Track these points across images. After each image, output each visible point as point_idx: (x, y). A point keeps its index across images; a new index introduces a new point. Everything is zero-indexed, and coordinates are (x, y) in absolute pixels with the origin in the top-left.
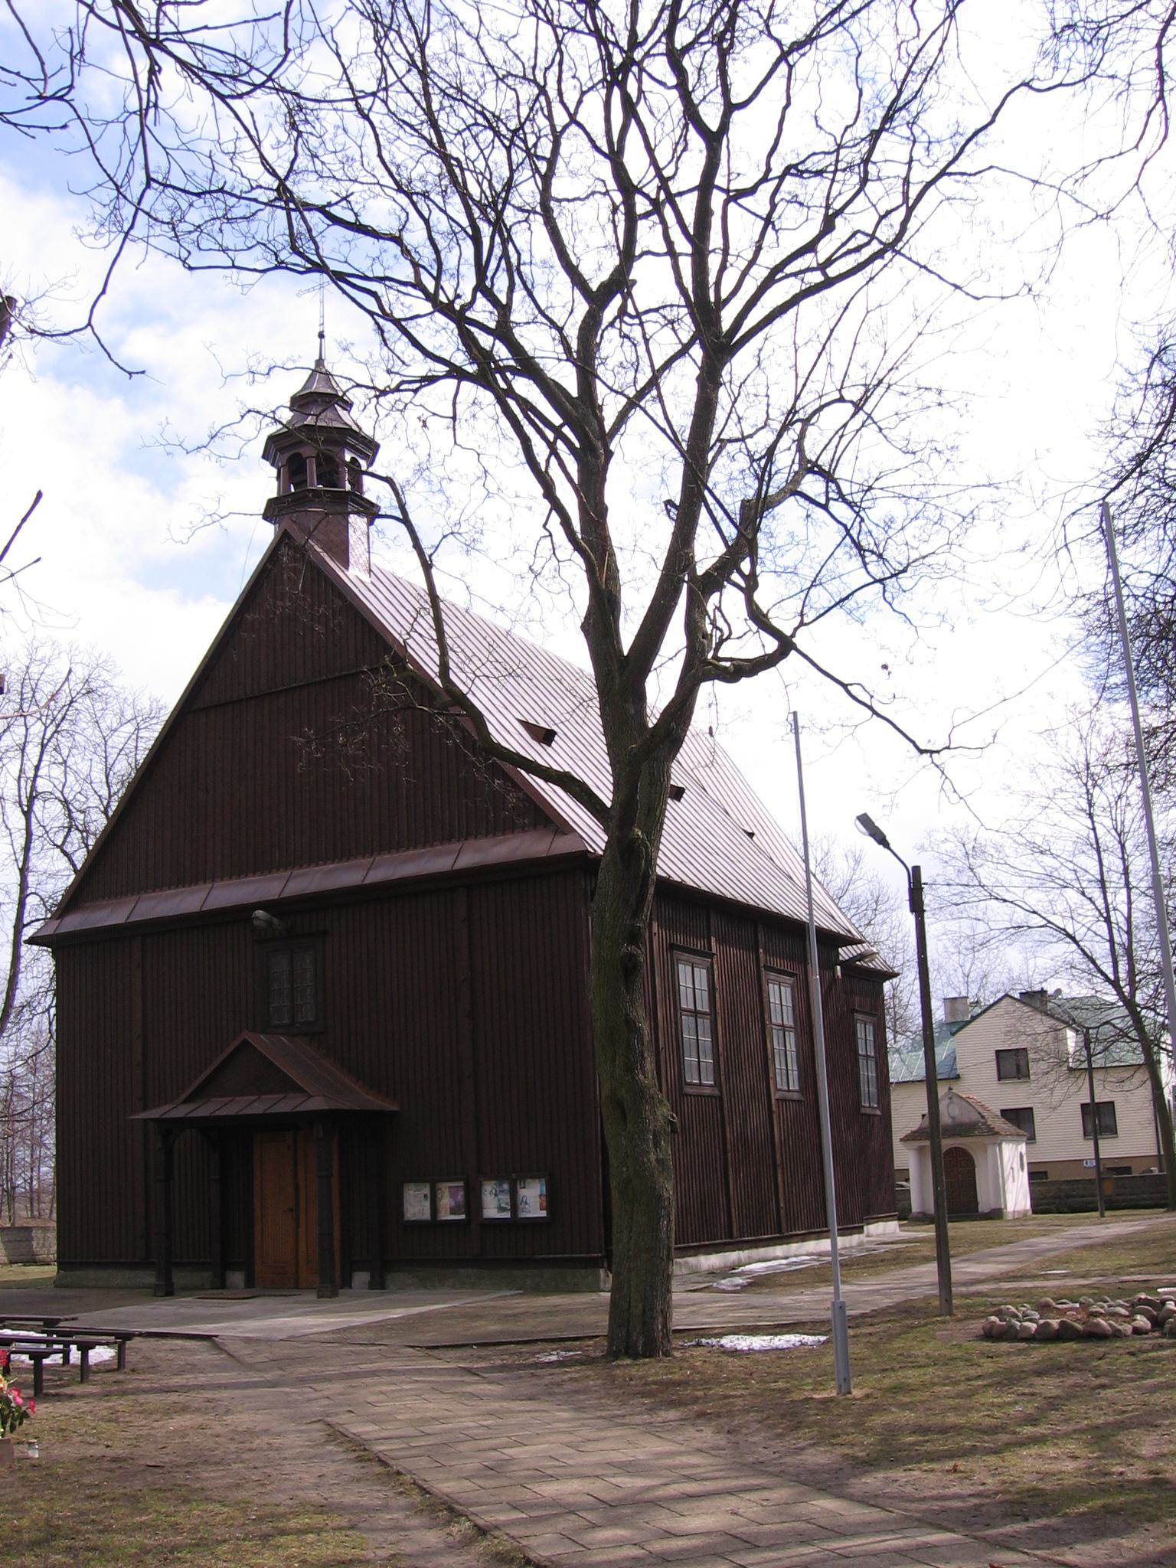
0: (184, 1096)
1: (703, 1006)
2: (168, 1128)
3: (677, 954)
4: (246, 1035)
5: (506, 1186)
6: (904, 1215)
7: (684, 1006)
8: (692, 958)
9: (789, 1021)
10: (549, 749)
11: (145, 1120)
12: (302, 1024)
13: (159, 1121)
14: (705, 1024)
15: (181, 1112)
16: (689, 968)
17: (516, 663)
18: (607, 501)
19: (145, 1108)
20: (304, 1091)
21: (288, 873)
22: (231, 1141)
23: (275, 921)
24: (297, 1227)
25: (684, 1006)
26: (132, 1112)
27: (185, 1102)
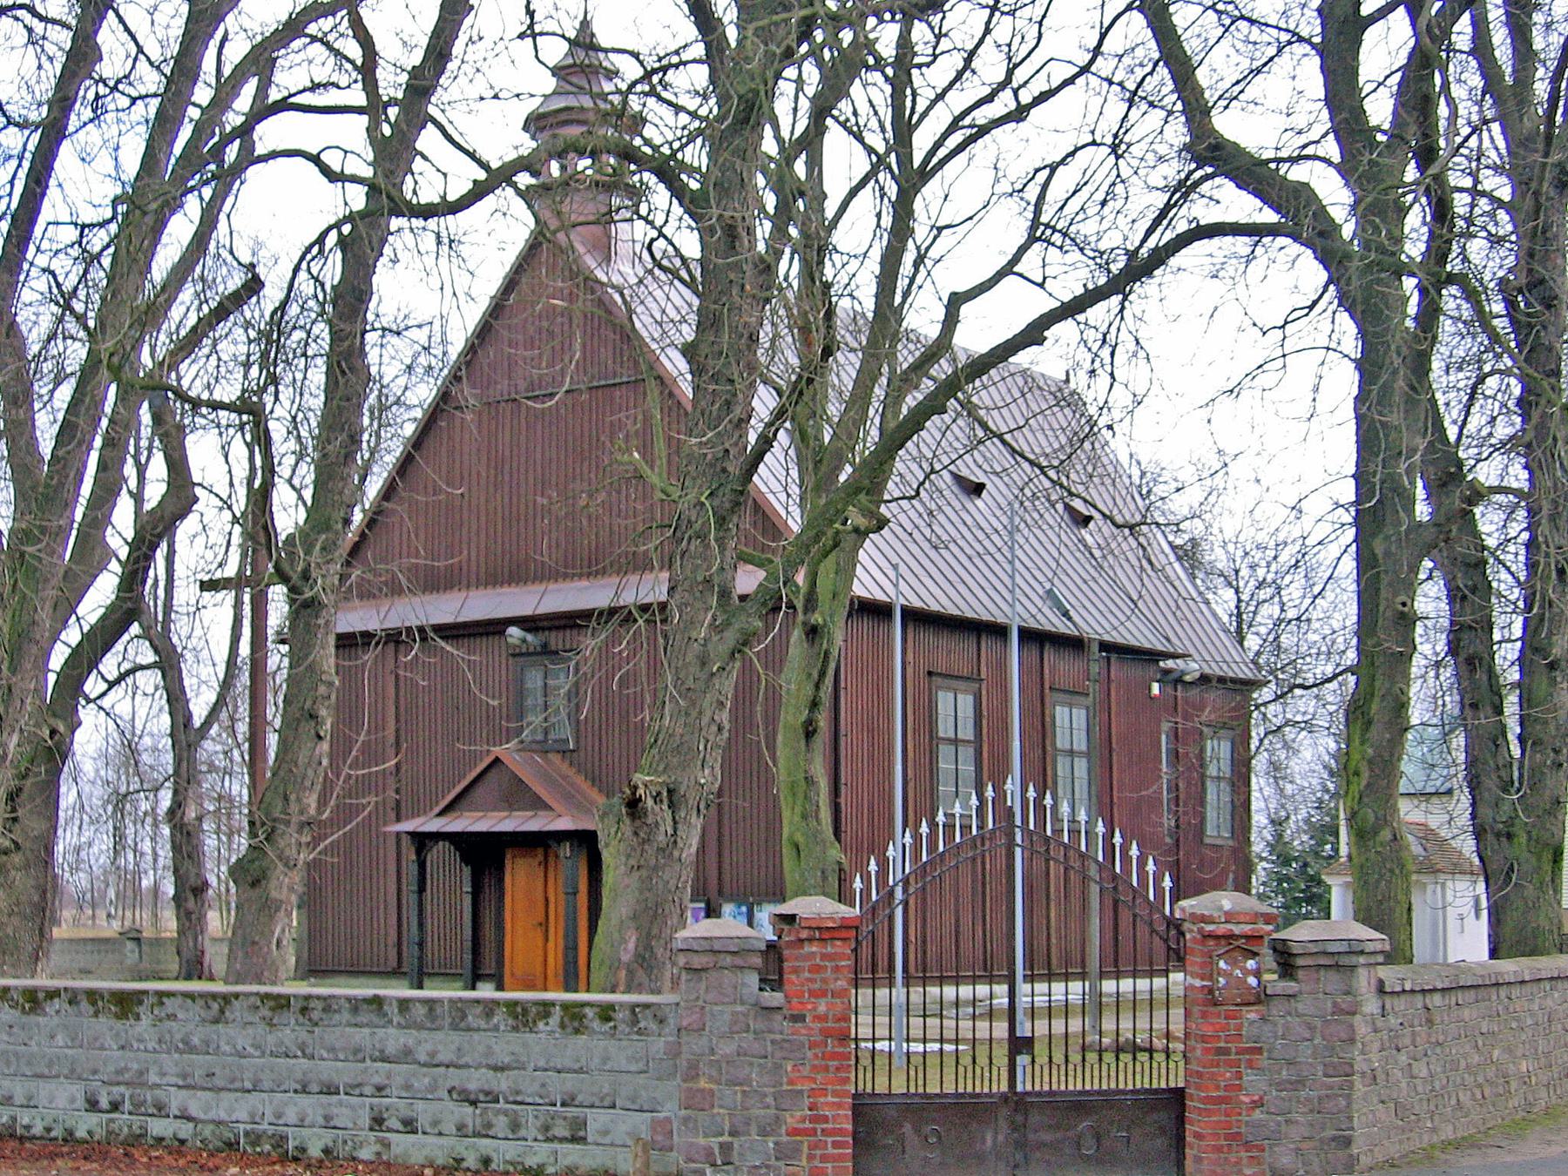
0: (437, 810)
1: (967, 733)
2: (422, 841)
3: (937, 680)
4: (496, 750)
5: (744, 909)
6: (1243, 886)
7: (941, 734)
8: (954, 683)
9: (1081, 744)
10: (969, 506)
11: (398, 834)
12: (555, 741)
13: (414, 835)
14: (967, 753)
15: (434, 825)
16: (951, 695)
17: (1236, 523)
18: (825, 188)
19: (398, 820)
20: (551, 809)
21: (543, 587)
22: (486, 855)
23: (530, 637)
24: (547, 940)
25: (941, 734)
26: (385, 824)
27: (440, 814)
